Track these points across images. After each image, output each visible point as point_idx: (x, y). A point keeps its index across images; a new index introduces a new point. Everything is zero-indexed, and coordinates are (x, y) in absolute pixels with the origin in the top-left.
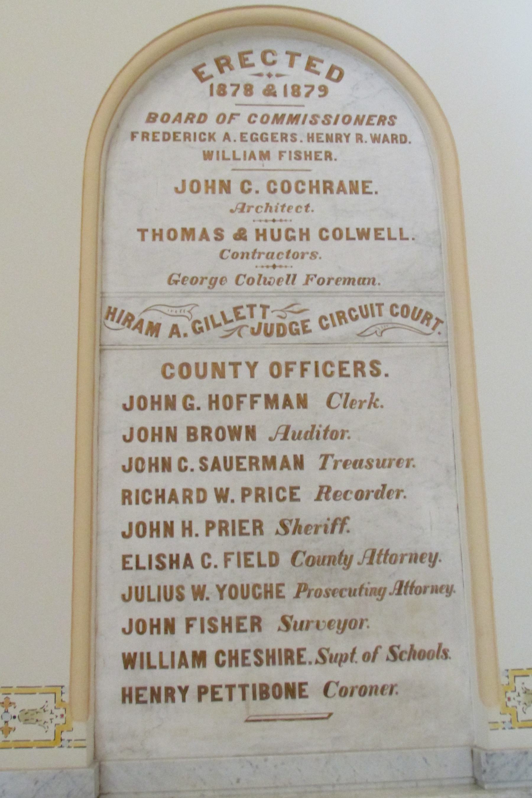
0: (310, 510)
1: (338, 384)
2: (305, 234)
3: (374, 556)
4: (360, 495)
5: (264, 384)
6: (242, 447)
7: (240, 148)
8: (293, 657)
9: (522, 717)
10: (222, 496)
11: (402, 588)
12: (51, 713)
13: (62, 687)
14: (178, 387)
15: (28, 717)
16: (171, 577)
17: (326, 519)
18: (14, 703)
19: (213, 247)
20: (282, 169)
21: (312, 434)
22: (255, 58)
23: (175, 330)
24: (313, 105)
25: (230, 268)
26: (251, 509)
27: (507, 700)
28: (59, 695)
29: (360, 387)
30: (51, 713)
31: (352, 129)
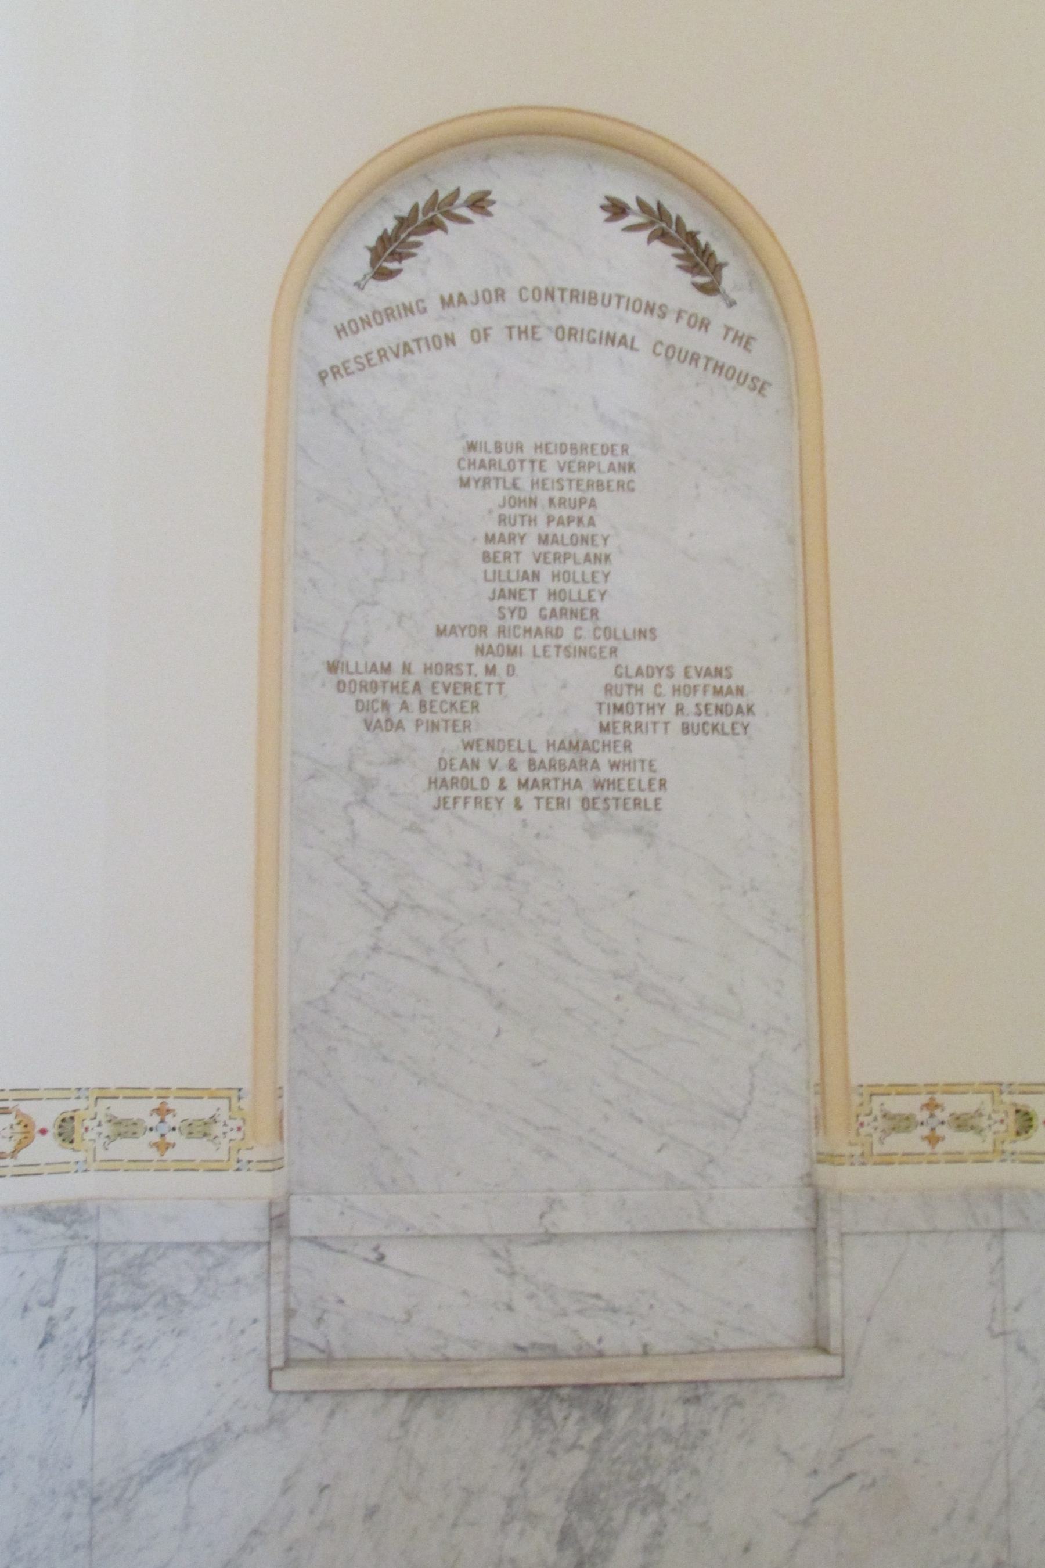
9: (877, 1149)
12: (225, 1125)
13: (240, 1090)
15: (962, 1123)
18: (173, 1110)
27: (83, 1130)
28: (234, 1100)
30: (225, 1125)
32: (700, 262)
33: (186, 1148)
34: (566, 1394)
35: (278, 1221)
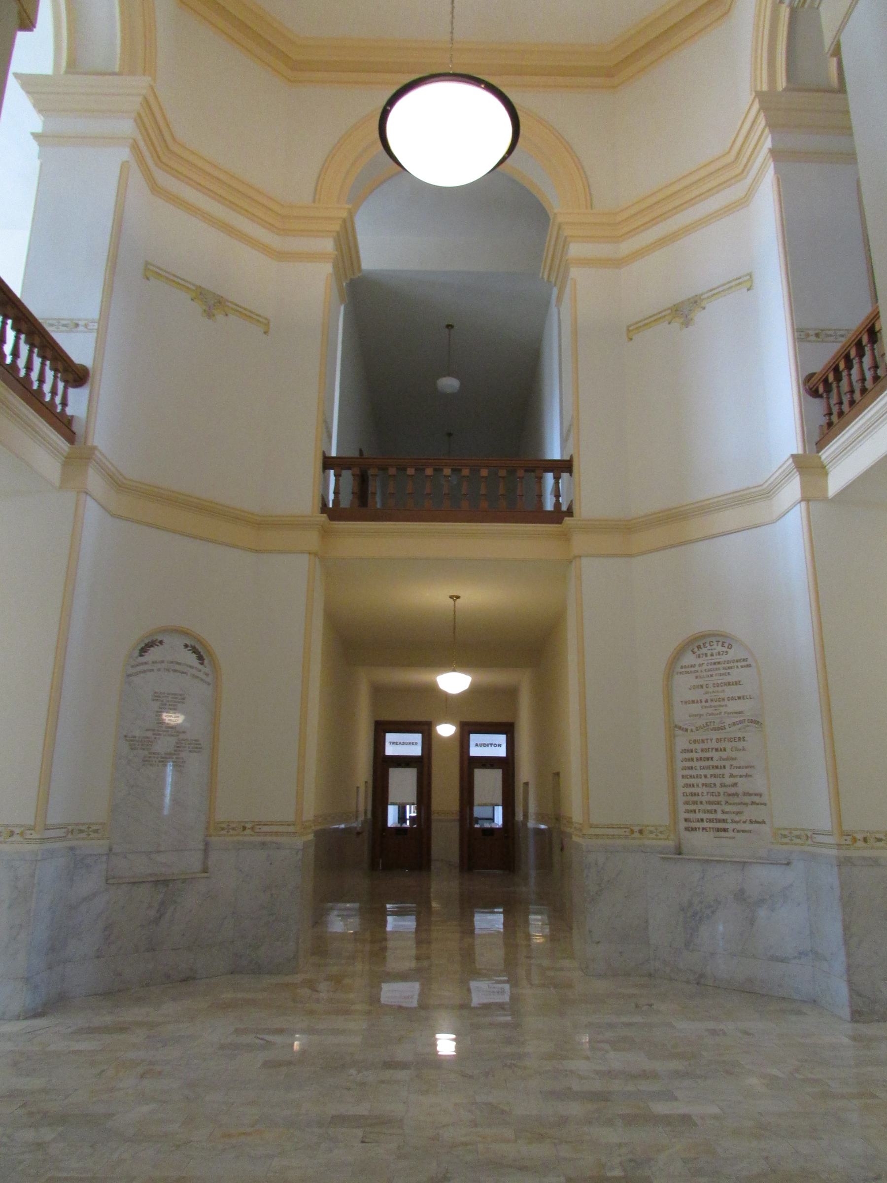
0: (728, 781)
1: (734, 744)
2: (724, 699)
3: (745, 794)
4: (741, 776)
5: (714, 745)
6: (710, 763)
7: (705, 674)
8: (724, 821)
10: (706, 776)
11: (753, 803)
14: (693, 746)
15: (233, 829)
16: (695, 798)
17: (299, 415)
19: (699, 705)
20: (717, 679)
21: (727, 759)
22: (707, 645)
23: (692, 731)
24: (724, 658)
25: (704, 711)
26: (713, 780)
29: (740, 745)
31: (736, 664)
32: (200, 658)
33: (93, 835)
34: (161, 882)
35: (111, 850)
